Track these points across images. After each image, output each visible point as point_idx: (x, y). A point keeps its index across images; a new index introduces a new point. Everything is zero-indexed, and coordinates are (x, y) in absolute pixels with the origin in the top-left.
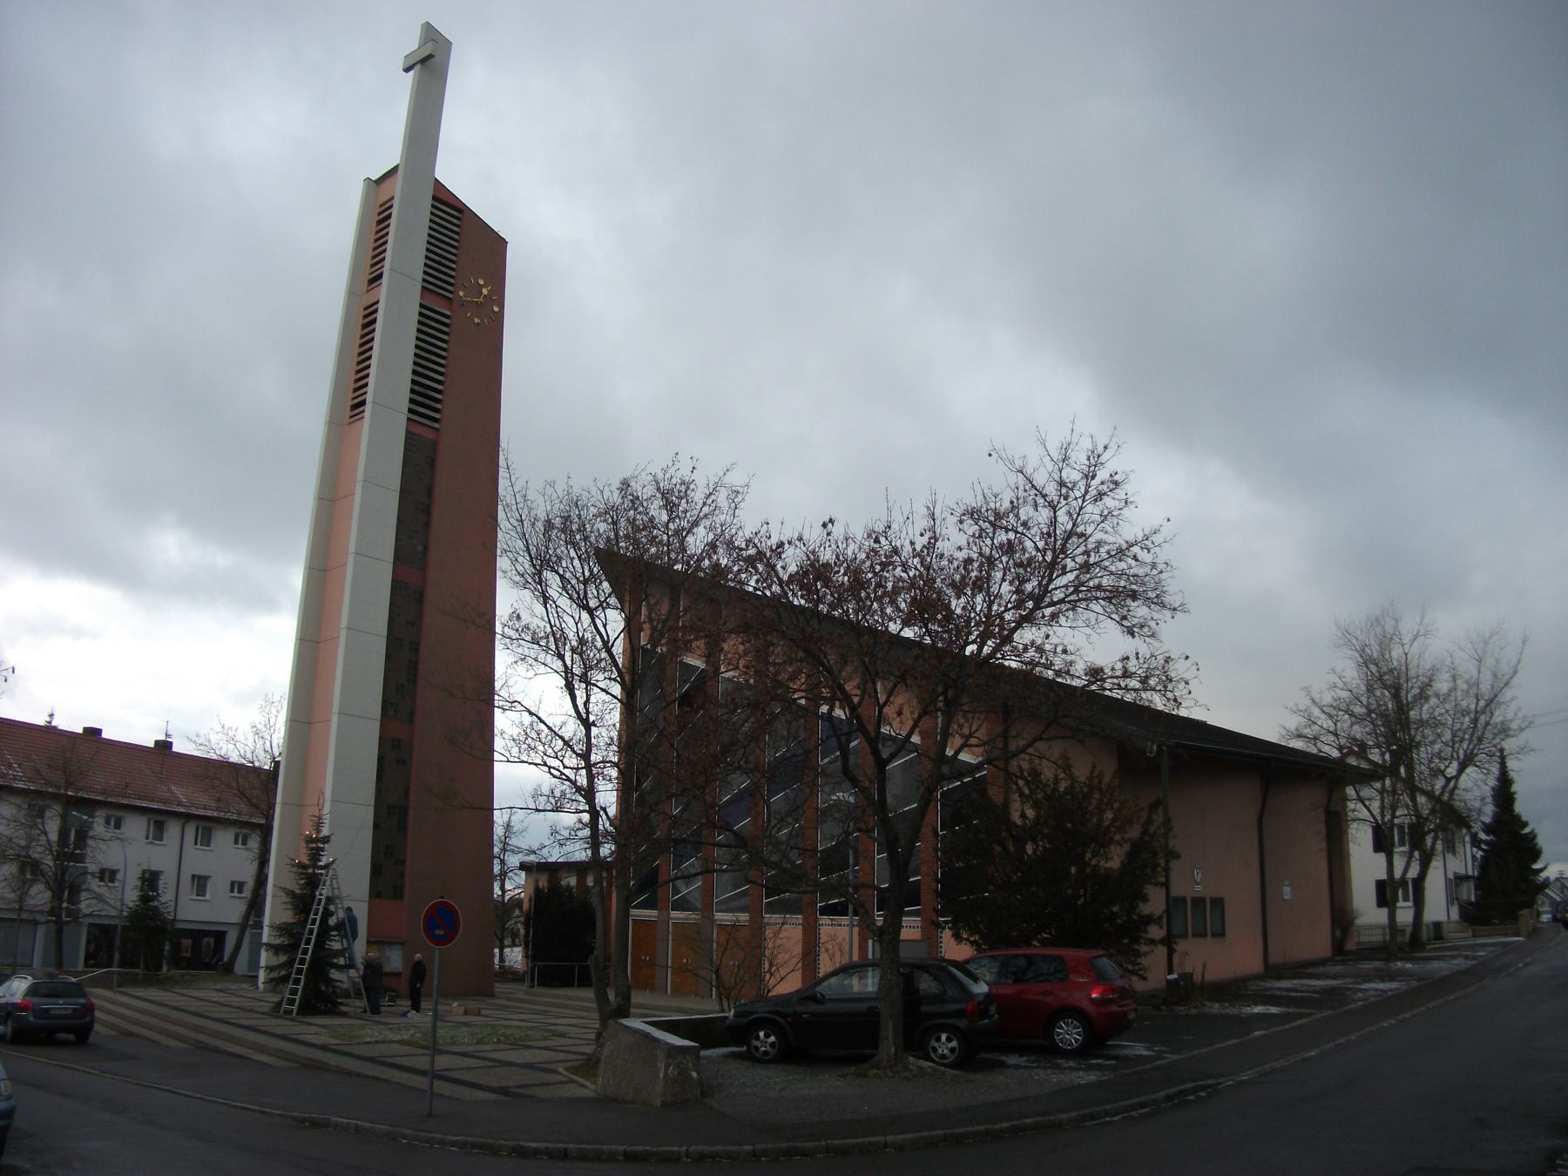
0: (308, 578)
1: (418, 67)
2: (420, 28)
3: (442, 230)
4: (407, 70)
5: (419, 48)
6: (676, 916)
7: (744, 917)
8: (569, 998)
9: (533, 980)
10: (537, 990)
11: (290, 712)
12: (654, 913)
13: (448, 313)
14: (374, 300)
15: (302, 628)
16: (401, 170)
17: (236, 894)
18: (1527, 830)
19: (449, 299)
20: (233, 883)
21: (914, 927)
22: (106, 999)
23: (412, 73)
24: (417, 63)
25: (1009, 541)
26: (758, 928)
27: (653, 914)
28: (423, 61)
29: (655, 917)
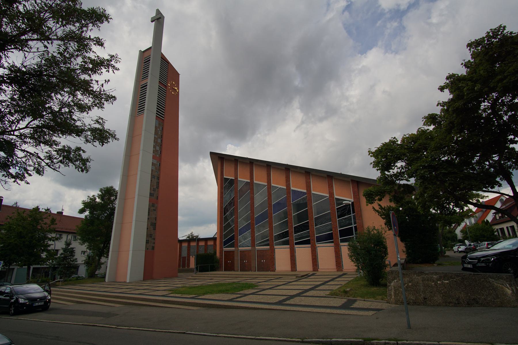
0: (133, 104)
1: (156, 21)
2: (156, 11)
3: (164, 63)
4: (152, 22)
5: (156, 15)
6: (257, 248)
7: (268, 247)
8: (211, 274)
9: (197, 270)
10: (198, 273)
11: (131, 108)
12: (234, 248)
13: (166, 89)
14: (149, 55)
15: (139, 62)
16: (152, 48)
17: (83, 255)
18: (74, 254)
19: (166, 86)
20: (82, 252)
21: (322, 247)
22: (55, 291)
23: (154, 22)
24: (155, 20)
25: (77, 267)
26: (273, 251)
27: (250, 248)
28: (158, 19)
29: (234, 250)
